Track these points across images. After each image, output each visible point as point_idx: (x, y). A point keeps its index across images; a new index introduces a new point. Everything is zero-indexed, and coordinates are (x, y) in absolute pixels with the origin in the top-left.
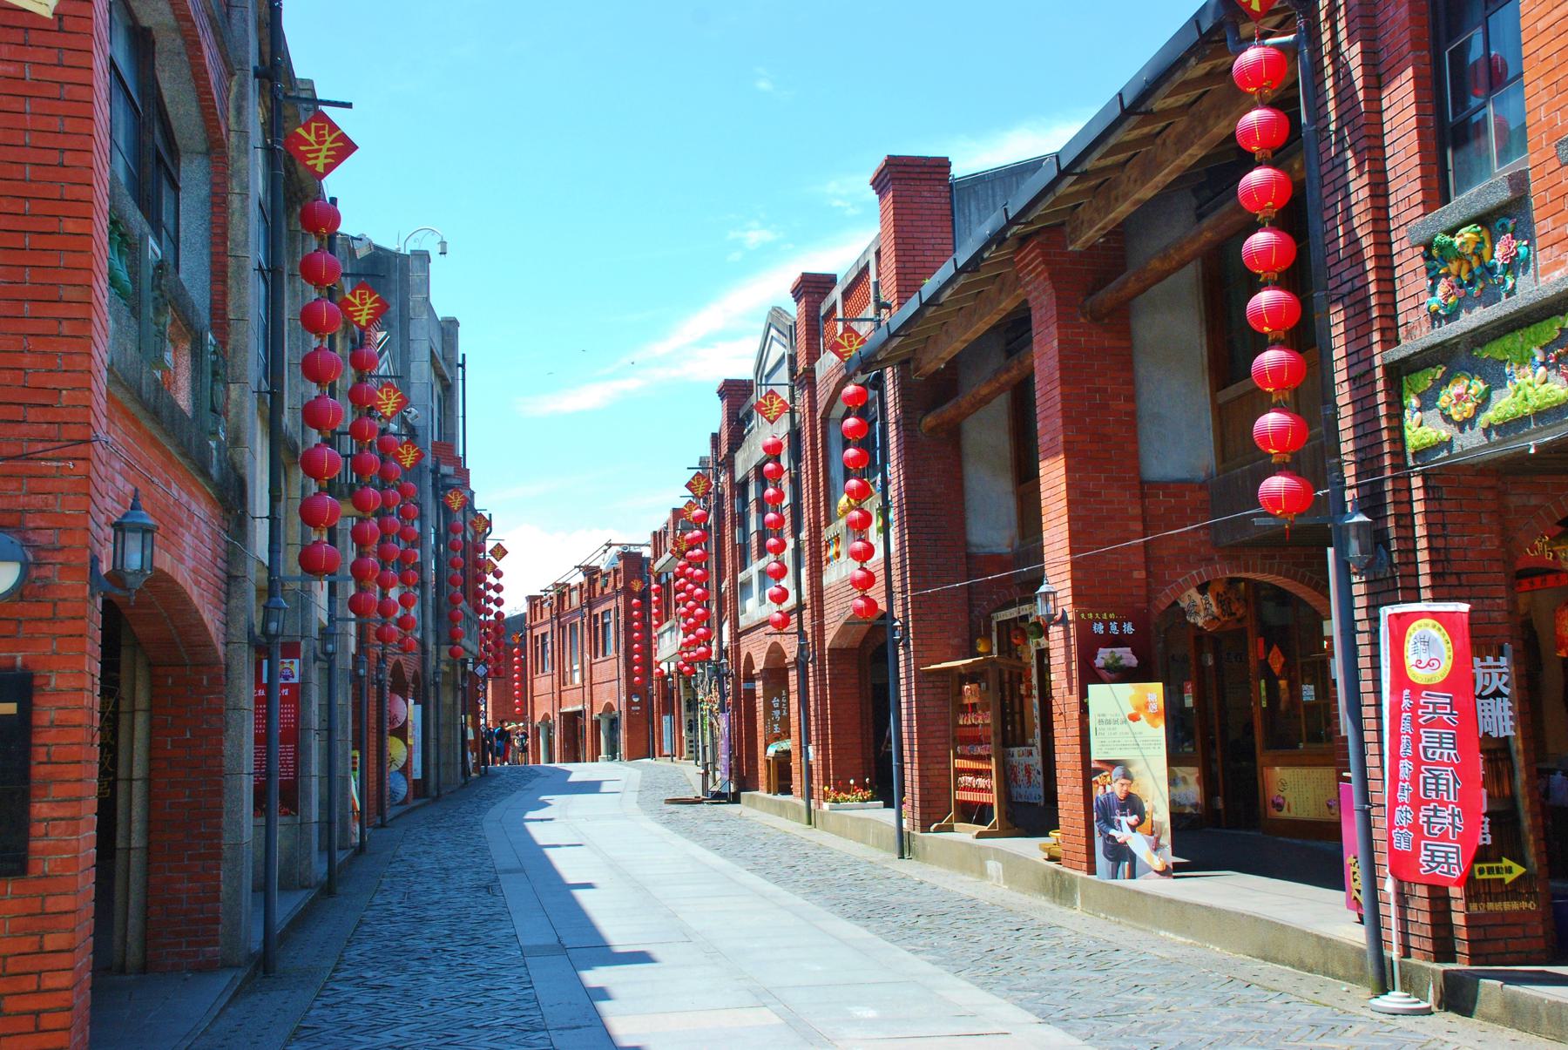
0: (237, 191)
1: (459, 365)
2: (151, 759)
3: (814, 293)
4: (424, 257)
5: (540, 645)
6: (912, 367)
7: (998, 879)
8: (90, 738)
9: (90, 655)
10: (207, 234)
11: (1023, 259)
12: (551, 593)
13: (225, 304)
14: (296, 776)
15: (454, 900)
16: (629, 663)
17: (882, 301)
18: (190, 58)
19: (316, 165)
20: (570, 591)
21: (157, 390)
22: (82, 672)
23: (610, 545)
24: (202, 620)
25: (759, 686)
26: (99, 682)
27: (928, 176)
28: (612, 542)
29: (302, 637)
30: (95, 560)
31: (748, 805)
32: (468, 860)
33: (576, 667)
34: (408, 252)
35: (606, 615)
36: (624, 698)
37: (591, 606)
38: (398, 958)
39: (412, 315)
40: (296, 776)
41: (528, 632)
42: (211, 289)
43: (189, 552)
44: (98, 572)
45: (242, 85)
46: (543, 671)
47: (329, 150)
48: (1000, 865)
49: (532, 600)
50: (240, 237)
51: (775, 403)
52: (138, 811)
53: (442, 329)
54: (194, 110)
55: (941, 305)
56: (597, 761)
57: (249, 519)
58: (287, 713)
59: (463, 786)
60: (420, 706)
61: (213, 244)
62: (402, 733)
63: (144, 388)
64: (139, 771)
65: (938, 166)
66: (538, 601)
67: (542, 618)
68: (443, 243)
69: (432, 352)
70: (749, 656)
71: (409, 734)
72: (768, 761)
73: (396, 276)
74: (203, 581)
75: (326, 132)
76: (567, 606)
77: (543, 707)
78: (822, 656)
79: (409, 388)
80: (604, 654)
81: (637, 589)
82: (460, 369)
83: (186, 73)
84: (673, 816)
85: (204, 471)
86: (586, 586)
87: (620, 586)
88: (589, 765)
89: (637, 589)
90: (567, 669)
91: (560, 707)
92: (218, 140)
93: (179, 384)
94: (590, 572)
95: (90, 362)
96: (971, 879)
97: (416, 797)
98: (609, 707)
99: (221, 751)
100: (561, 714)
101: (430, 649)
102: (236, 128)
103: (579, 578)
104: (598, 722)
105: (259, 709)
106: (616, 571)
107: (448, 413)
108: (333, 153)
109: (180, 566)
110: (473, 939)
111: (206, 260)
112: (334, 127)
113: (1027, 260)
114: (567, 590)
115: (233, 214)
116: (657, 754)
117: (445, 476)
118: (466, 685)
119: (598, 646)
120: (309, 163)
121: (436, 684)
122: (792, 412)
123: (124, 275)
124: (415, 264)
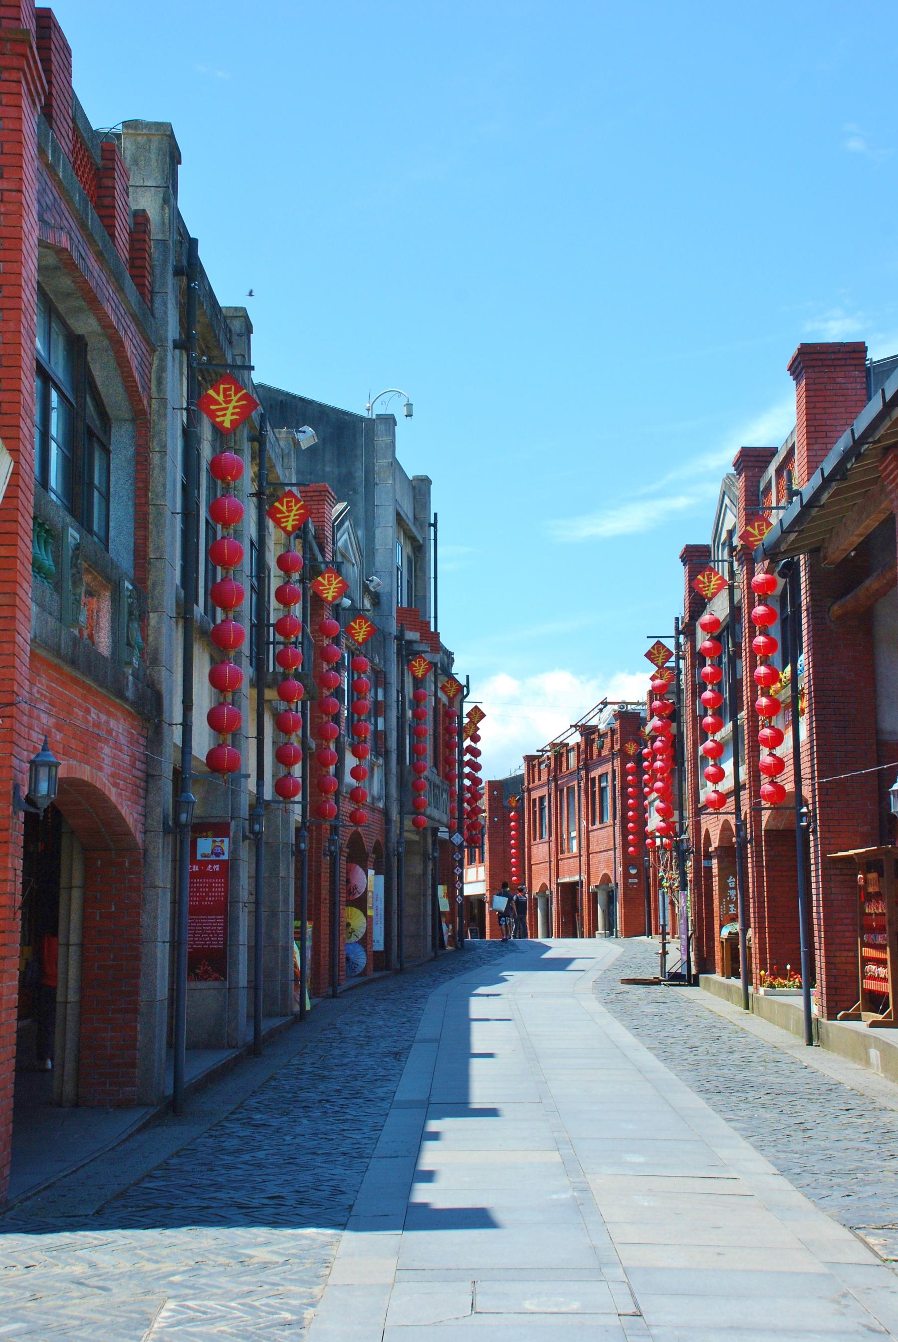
0: (157, 449)
1: (431, 525)
2: (85, 930)
3: (755, 467)
4: (389, 421)
5: (537, 809)
6: (822, 555)
7: (878, 1068)
8: (12, 915)
9: (13, 855)
10: (132, 488)
11: (886, 467)
12: (549, 754)
13: (146, 546)
14: (225, 944)
15: (360, 1063)
16: (625, 832)
17: (795, 487)
18: (116, 353)
19: (223, 422)
20: (568, 751)
21: (75, 645)
22: (6, 868)
23: (605, 703)
24: (121, 814)
25: (715, 862)
26: (21, 874)
27: (843, 362)
28: (608, 700)
29: (232, 818)
30: (16, 787)
31: (704, 989)
32: (395, 1029)
33: (574, 834)
34: (374, 417)
35: (604, 778)
36: (620, 869)
37: (588, 769)
38: (287, 1106)
39: (377, 481)
40: (225, 944)
41: (526, 794)
42: (135, 534)
43: (107, 761)
44: (19, 797)
45: (162, 360)
46: (541, 837)
47: (235, 407)
48: (878, 1053)
49: (529, 759)
50: (160, 489)
51: (713, 579)
52: (73, 972)
53: (414, 488)
54: (120, 390)
55: (823, 506)
56: (594, 937)
57: (166, 726)
58: (218, 887)
59: (431, 960)
60: (382, 877)
61: (137, 496)
62: (361, 903)
63: (63, 646)
64: (74, 938)
65: (854, 352)
66: (536, 762)
67: (539, 779)
68: (409, 406)
69: (398, 514)
70: (707, 831)
71: (369, 905)
72: (722, 942)
73: (362, 441)
74: (122, 782)
75: (293, 504)
76: (564, 769)
77: (540, 878)
78: (758, 837)
79: (374, 554)
80: (601, 821)
81: (631, 752)
82: (432, 528)
83: (113, 363)
84: (620, 997)
85: (121, 695)
86: (582, 747)
87: (617, 747)
88: (586, 940)
89: (631, 752)
90: (565, 836)
91: (558, 877)
92: (141, 410)
93: (102, 625)
94: (587, 731)
95: (14, 647)
96: (859, 1067)
97: (376, 969)
98: (606, 879)
99: (138, 922)
100: (558, 884)
101: (394, 818)
102: (157, 396)
103: (575, 738)
104: (595, 895)
105: (193, 883)
106: (613, 731)
107: (419, 574)
108: (297, 517)
109: (100, 774)
110: (357, 1093)
111: (131, 509)
112: (480, 710)
113: (888, 471)
114: (564, 750)
115: (153, 469)
116: (653, 932)
117: (410, 642)
118: (436, 854)
119: (595, 814)
120: (218, 420)
121: (399, 854)
122: (731, 589)
123: (48, 562)
124: (380, 428)
